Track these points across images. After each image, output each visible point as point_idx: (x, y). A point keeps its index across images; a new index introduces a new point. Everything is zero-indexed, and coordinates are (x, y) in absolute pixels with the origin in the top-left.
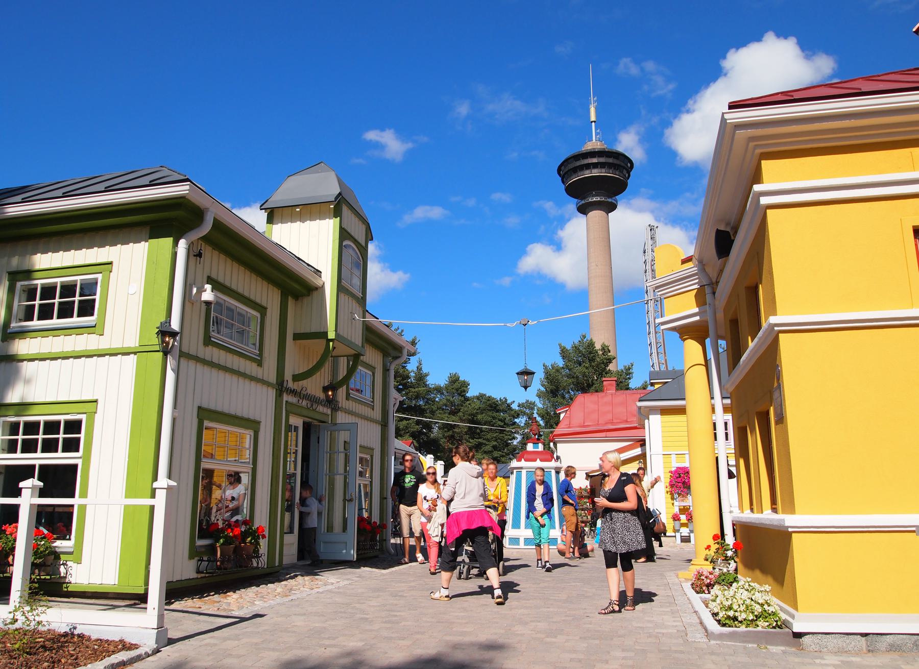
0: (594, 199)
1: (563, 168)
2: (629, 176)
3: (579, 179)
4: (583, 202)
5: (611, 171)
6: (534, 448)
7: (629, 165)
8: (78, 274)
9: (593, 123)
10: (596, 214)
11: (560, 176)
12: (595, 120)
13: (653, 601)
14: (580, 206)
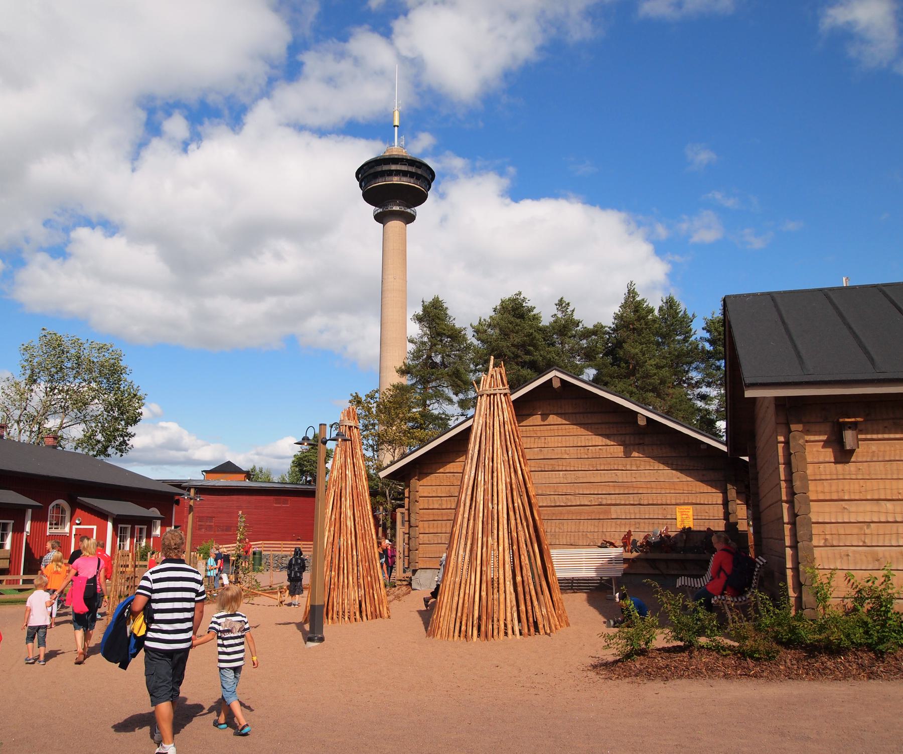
3: (386, 184)
6: (611, 508)
8: (760, 381)
9: (396, 128)
10: (395, 225)
11: (358, 181)
12: (398, 125)
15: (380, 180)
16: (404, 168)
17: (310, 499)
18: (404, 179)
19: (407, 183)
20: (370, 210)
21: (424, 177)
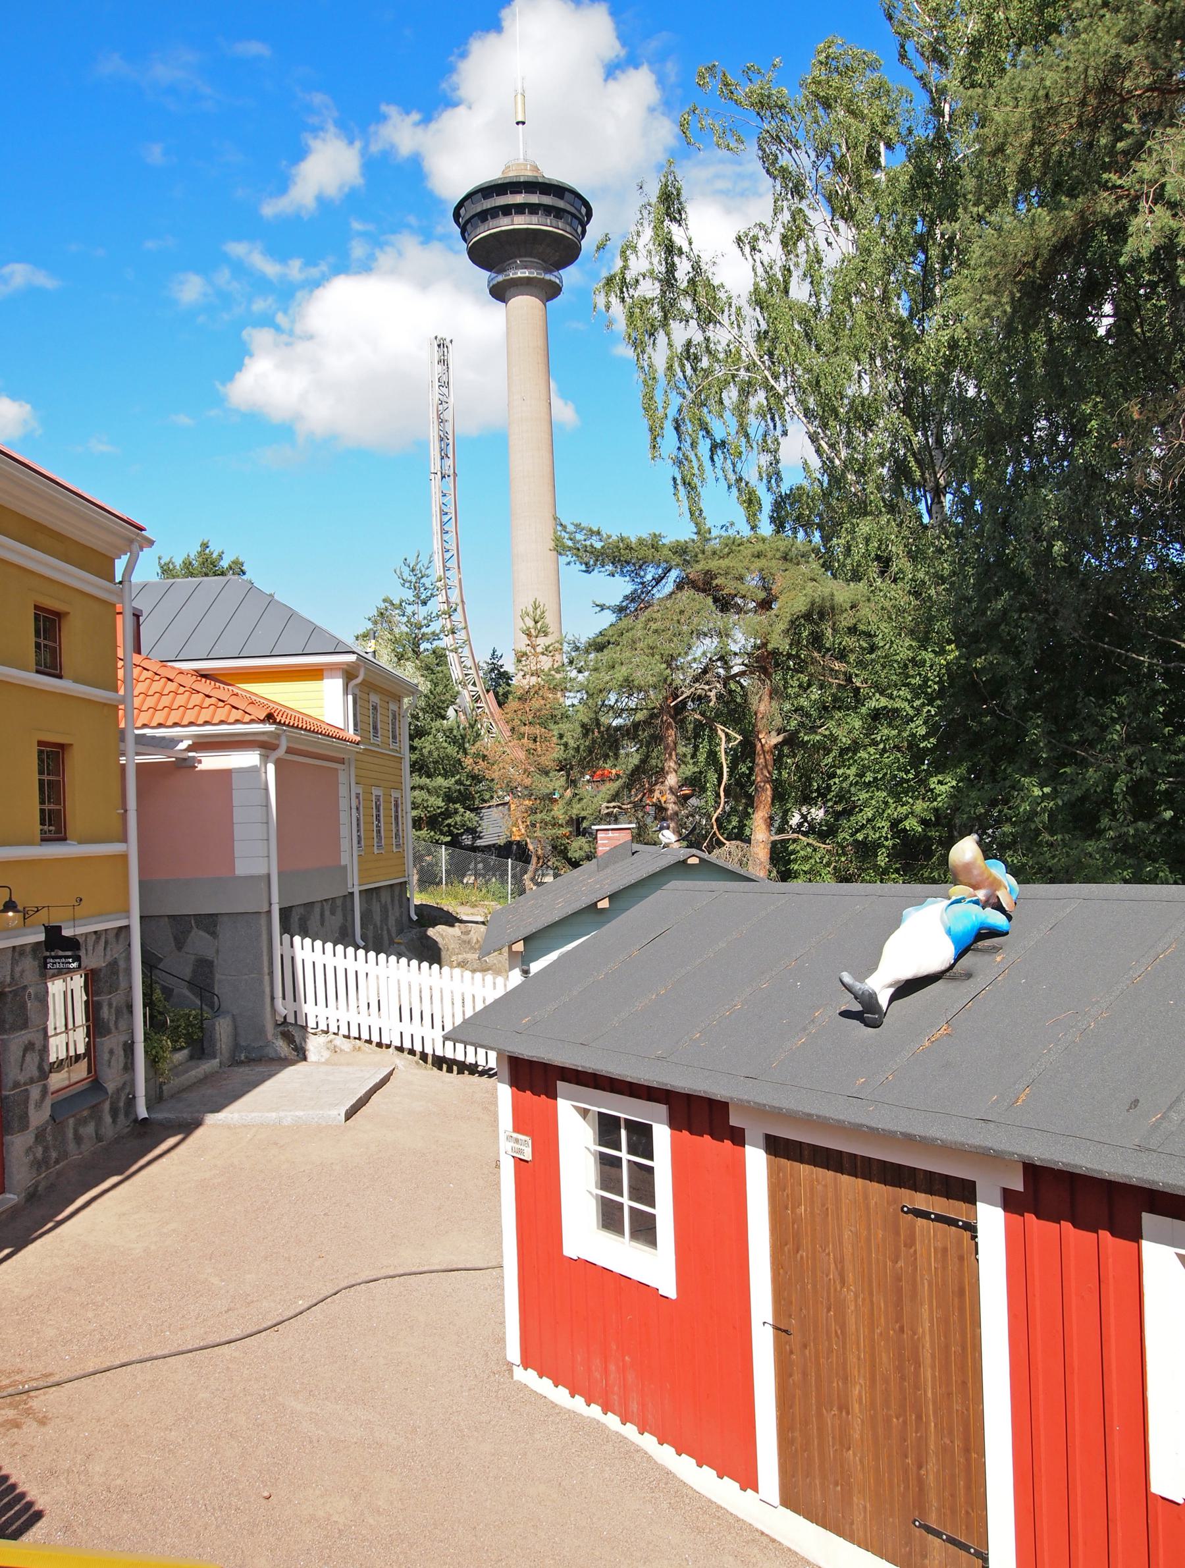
0: (519, 275)
1: (462, 211)
2: (584, 232)
3: (490, 234)
4: (501, 278)
5: (548, 221)
7: (584, 210)
13: (573, 1396)
14: (494, 286)
15: (482, 228)
16: (534, 199)
17: (236, 781)
18: (535, 219)
19: (525, 226)
20: (482, 277)
21: (569, 212)
